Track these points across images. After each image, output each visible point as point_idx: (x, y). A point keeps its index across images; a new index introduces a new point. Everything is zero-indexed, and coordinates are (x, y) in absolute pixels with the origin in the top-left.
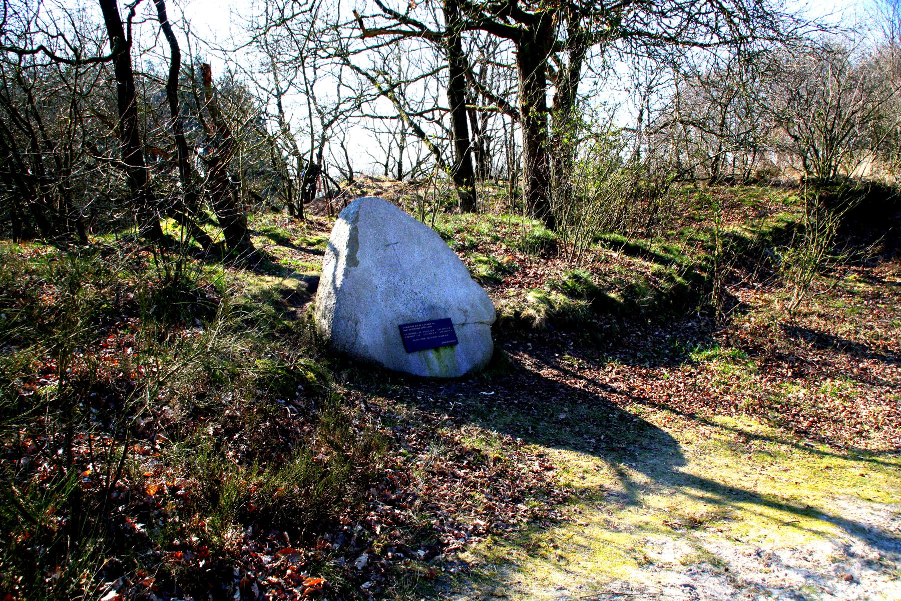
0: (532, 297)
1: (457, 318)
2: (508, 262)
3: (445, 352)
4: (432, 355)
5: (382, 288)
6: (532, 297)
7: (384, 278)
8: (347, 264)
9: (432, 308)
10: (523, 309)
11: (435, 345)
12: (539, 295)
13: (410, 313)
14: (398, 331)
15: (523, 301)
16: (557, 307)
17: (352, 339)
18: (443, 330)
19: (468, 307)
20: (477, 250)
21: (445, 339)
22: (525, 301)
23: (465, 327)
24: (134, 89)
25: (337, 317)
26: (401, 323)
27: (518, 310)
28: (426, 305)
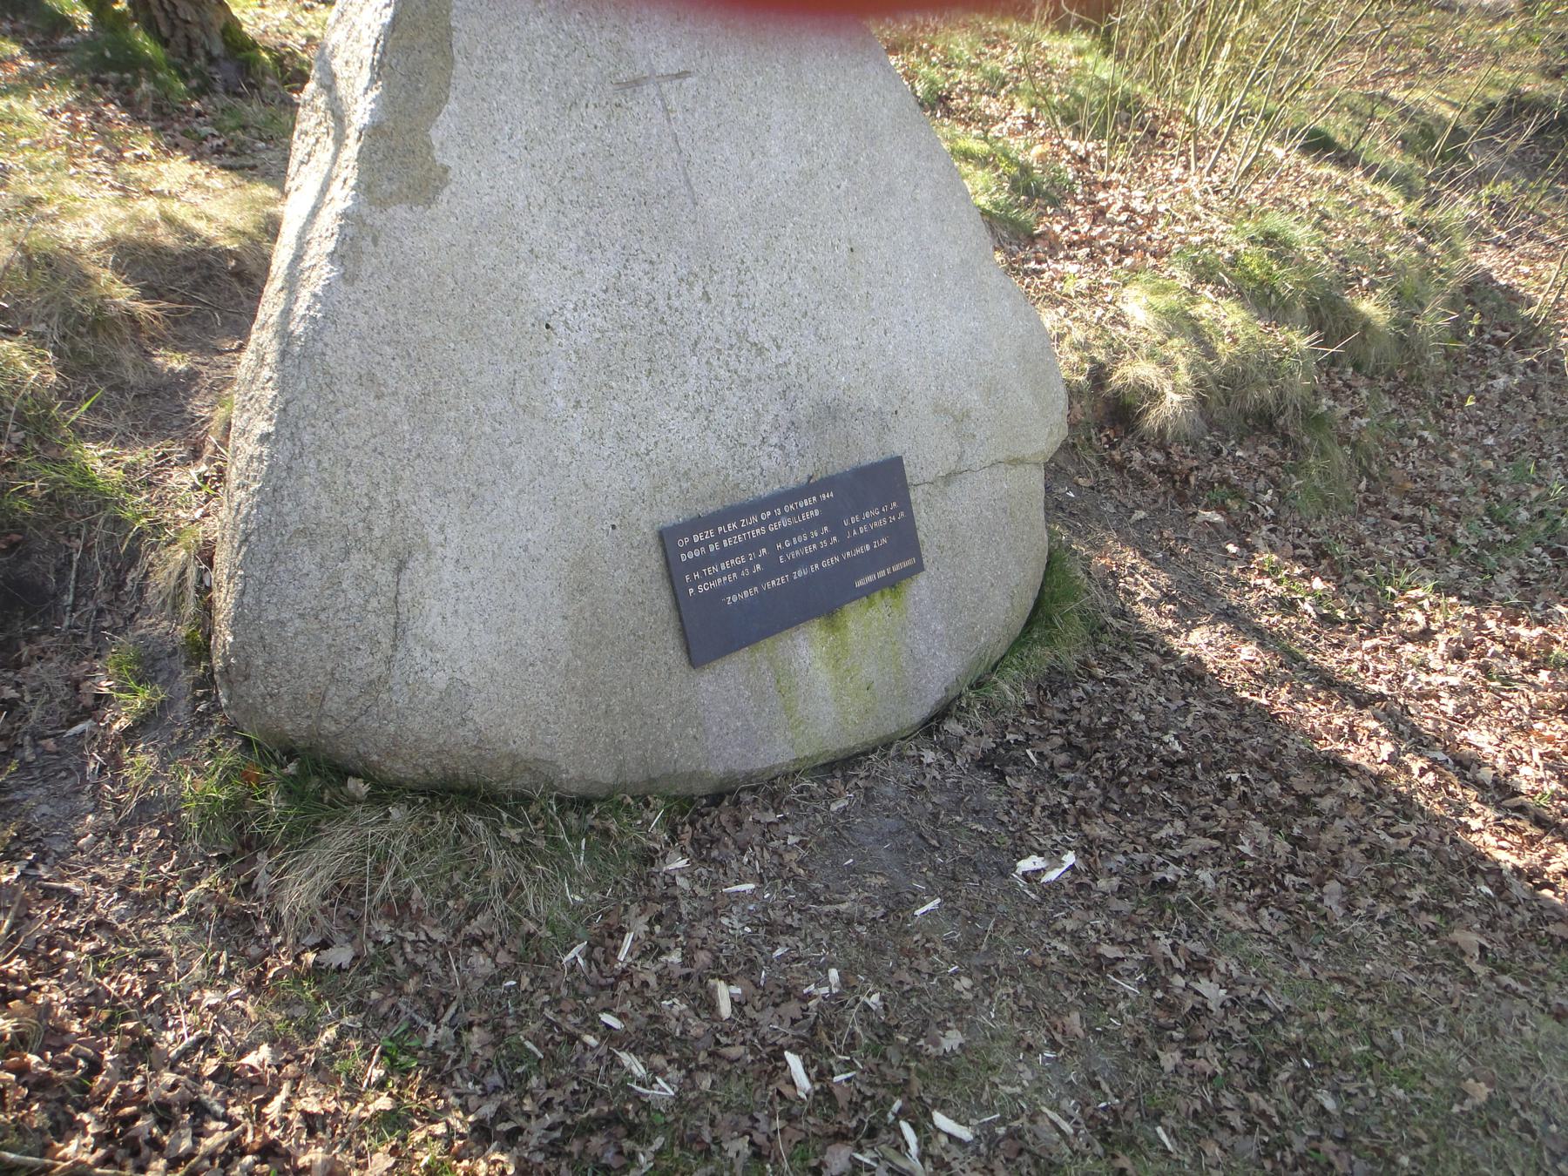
0: (1139, 306)
1: (924, 452)
2: (1042, 158)
3: (865, 622)
4: (807, 649)
5: (214, 1061)
6: (1139, 306)
7: (598, 274)
8: (366, 187)
9: (830, 413)
10: (1117, 352)
11: (821, 601)
12: (1161, 302)
13: (720, 455)
14: (655, 562)
15: (1114, 321)
16: (1223, 348)
17: (364, 663)
18: (875, 518)
19: (973, 398)
20: (949, 112)
21: (872, 562)
22: (1119, 319)
23: (954, 488)
24: (1471, 580)
25: (266, 538)
26: (671, 515)
27: (1101, 356)
28: (804, 406)
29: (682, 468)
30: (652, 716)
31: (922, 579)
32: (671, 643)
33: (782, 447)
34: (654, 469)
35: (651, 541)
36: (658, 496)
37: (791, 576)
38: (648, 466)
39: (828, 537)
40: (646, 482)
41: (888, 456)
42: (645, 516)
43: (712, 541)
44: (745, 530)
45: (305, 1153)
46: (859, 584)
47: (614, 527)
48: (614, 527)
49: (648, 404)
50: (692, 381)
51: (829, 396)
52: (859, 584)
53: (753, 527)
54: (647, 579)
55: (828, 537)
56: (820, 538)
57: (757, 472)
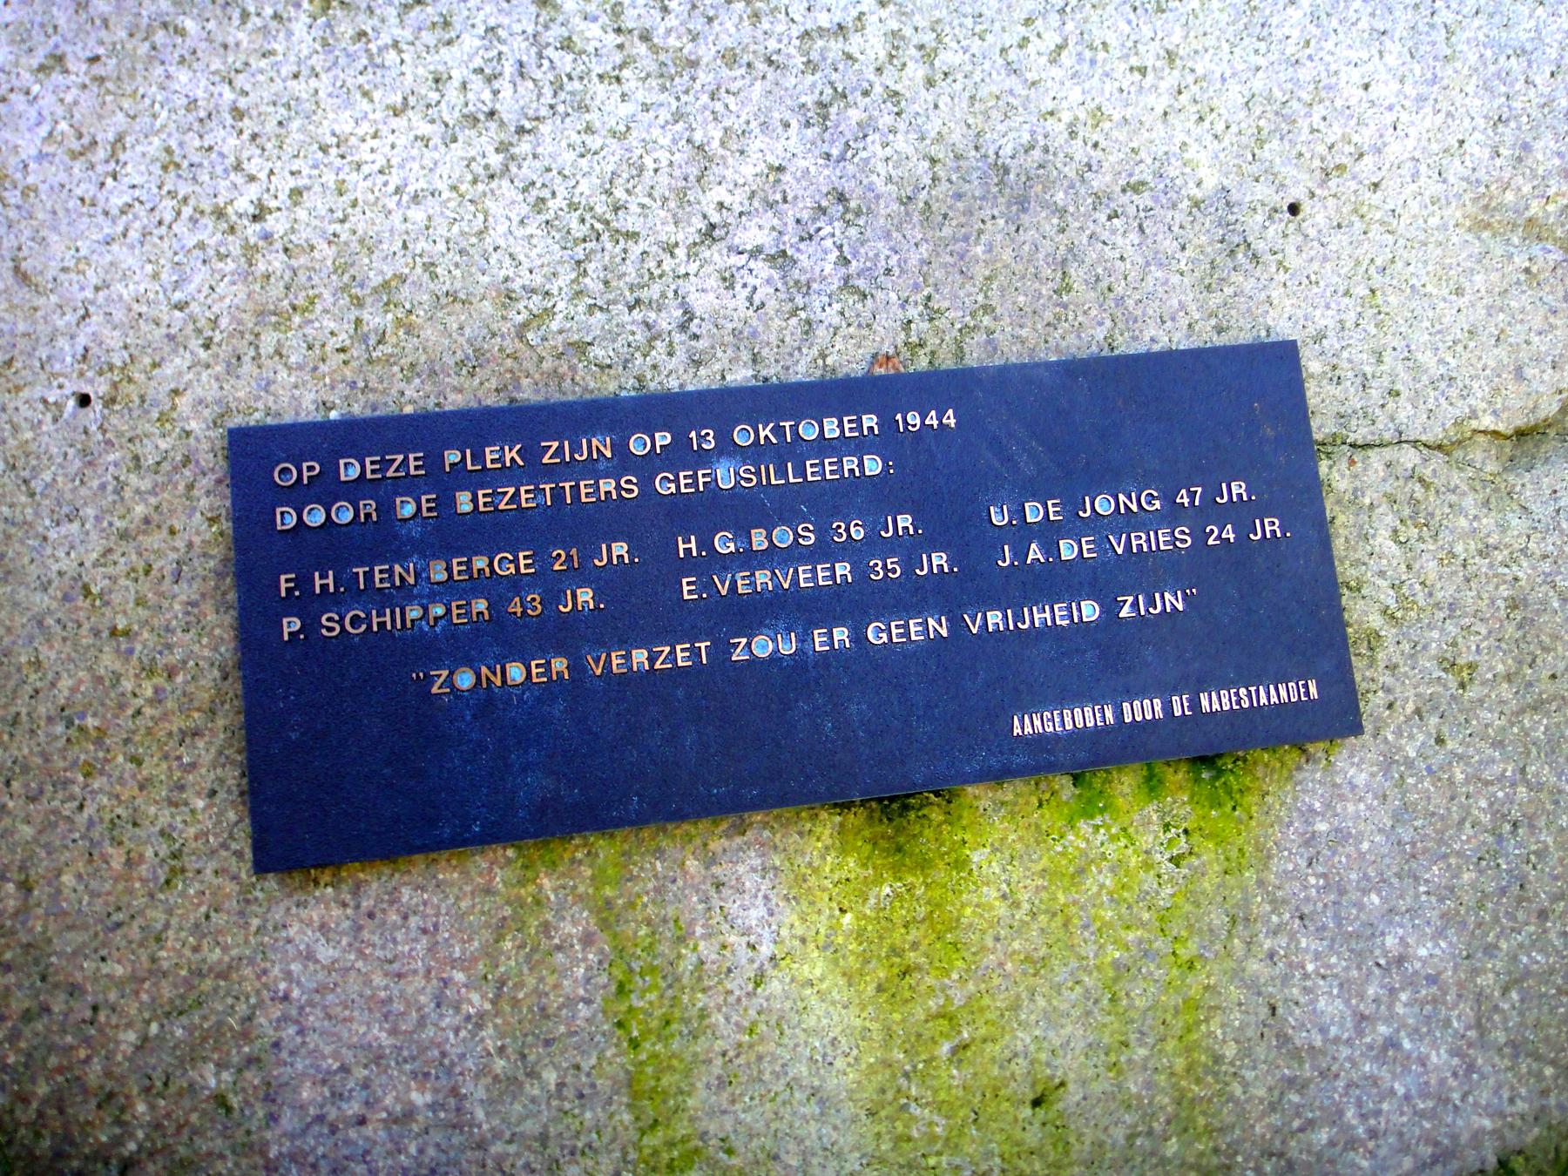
11: (880, 757)
26: (297, 397)
29: (377, 270)
30: (74, 990)
31: (1353, 764)
32: (205, 777)
33: (781, 259)
34: (275, 262)
35: (206, 459)
36: (269, 340)
37: (722, 649)
38: (250, 251)
39: (910, 549)
40: (232, 294)
41: (1241, 334)
42: (206, 386)
43: (408, 486)
44: (550, 472)
45: (992, 908)
46: (1026, 726)
47: (84, 400)
48: (84, 400)
49: (300, 88)
50: (470, 42)
51: (1006, 139)
52: (1026, 726)
53: (592, 469)
54: (165, 564)
55: (910, 549)
56: (874, 543)
57: (667, 320)
